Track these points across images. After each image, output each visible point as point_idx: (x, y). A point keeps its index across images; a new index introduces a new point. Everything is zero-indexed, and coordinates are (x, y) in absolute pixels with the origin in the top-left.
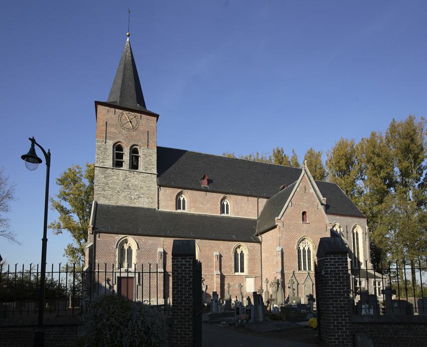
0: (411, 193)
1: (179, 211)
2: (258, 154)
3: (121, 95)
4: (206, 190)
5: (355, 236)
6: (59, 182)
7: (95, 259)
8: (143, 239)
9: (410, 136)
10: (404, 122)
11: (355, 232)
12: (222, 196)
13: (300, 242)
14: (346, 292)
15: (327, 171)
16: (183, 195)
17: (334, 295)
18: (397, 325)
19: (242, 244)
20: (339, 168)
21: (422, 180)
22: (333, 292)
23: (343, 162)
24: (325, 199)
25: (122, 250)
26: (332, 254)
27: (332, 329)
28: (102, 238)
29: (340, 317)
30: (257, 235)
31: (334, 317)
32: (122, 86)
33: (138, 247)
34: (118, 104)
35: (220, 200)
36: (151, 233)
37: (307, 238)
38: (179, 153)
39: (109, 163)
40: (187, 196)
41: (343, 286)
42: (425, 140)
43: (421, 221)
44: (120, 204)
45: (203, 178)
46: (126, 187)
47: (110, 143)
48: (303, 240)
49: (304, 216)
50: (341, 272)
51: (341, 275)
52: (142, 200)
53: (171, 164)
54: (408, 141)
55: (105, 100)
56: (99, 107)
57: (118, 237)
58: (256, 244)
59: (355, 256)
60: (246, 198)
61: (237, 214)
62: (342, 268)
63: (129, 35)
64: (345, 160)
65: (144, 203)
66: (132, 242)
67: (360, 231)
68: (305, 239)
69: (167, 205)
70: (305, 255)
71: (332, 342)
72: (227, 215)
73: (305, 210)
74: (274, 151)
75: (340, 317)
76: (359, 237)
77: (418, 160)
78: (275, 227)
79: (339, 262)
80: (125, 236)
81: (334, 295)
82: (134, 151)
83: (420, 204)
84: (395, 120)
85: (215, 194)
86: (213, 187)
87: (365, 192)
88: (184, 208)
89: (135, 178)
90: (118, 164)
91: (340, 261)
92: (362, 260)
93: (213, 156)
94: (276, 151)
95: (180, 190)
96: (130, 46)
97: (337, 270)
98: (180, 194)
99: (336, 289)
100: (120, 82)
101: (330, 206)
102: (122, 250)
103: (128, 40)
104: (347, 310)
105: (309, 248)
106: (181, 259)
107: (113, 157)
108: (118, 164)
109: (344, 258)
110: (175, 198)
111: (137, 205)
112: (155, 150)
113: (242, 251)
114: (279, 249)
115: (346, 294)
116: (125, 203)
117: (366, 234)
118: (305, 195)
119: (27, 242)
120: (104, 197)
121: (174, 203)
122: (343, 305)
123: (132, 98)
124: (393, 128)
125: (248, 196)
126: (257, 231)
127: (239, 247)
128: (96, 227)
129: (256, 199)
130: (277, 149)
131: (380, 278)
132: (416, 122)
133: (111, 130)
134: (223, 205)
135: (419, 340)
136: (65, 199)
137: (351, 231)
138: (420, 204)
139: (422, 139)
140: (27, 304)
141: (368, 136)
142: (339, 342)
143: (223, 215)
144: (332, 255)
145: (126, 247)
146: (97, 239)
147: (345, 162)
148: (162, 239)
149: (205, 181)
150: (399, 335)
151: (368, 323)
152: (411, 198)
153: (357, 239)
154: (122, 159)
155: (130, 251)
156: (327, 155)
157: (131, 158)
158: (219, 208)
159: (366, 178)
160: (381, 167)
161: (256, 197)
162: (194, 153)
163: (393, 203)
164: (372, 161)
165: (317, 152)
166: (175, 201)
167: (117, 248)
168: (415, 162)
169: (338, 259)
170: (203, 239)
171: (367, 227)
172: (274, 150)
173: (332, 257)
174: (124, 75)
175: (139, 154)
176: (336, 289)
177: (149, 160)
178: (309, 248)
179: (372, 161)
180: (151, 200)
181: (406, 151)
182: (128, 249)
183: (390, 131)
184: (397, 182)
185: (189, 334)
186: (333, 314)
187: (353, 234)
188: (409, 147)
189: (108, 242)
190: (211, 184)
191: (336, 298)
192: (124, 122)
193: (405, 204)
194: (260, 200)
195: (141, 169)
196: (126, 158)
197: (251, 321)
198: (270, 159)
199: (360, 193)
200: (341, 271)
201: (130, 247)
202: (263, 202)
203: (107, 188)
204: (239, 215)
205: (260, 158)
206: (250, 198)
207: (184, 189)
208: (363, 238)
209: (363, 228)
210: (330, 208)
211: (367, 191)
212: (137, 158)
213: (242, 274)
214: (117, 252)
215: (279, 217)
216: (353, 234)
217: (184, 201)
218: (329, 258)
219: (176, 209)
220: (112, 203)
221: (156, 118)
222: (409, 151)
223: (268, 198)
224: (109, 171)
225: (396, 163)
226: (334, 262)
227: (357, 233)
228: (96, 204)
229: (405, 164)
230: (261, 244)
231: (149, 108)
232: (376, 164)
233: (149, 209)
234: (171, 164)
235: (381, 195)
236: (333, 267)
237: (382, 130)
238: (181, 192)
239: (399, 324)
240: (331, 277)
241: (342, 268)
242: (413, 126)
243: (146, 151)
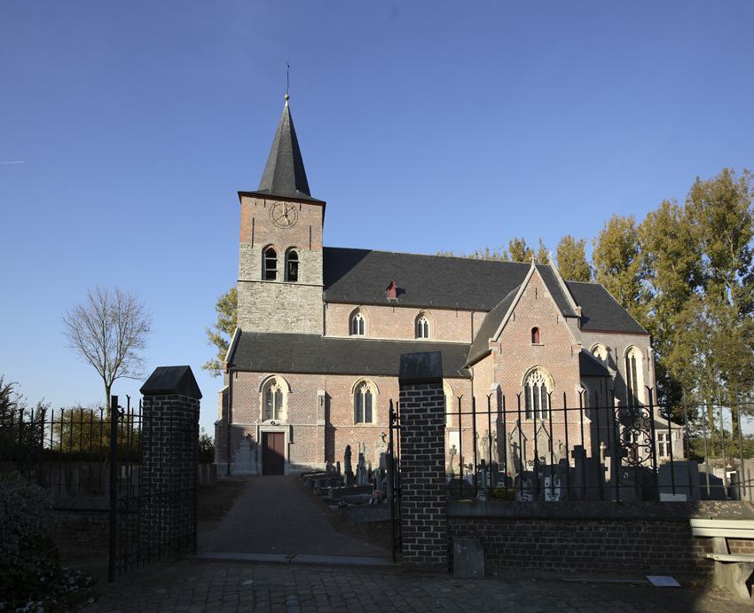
0: (729, 295)
1: (354, 336)
2: (488, 250)
3: (274, 180)
4: (393, 305)
5: (631, 364)
6: (219, 308)
7: (231, 407)
8: (297, 379)
9: (727, 200)
10: (715, 181)
11: (630, 356)
12: (417, 311)
13: (528, 375)
14: (438, 457)
15: (594, 268)
16: (360, 314)
17: (416, 463)
18: (542, 522)
19: (366, 378)
20: (611, 260)
21: (749, 271)
22: (412, 458)
23: (617, 251)
24: (580, 308)
25: (268, 395)
26: (412, 384)
27: (409, 528)
28: (242, 378)
29: (424, 505)
30: (467, 368)
31: (413, 505)
32: (276, 168)
33: (290, 389)
34: (270, 193)
35: (414, 318)
36: (307, 370)
37: (540, 369)
38: (359, 255)
39: (257, 275)
40: (366, 314)
41: (432, 445)
42: (752, 207)
43: (745, 335)
44: (272, 330)
45: (390, 287)
46: (280, 307)
47: (259, 247)
48: (533, 372)
49: (536, 335)
50: (429, 420)
51: (430, 424)
52: (302, 324)
53: (343, 269)
54: (722, 210)
55: (254, 189)
56: (244, 198)
57: (262, 376)
58: (464, 381)
59: (630, 391)
60: (453, 313)
61: (441, 337)
62: (432, 410)
63: (288, 98)
64: (620, 248)
65: (306, 327)
66: (281, 381)
67: (637, 354)
68: (536, 370)
69: (337, 329)
70: (538, 396)
71: (408, 553)
72: (426, 340)
73: (537, 325)
74: (511, 245)
75: (424, 505)
76: (638, 364)
77: (742, 239)
78: (489, 353)
79: (427, 399)
80: (269, 374)
81: (416, 463)
82: (292, 256)
83: (744, 310)
84: (700, 180)
85: (407, 310)
86: (405, 298)
87: (655, 297)
88: (362, 333)
89: (293, 293)
90: (269, 275)
91: (429, 397)
92: (642, 397)
93: (407, 255)
94: (513, 244)
95: (355, 307)
96: (290, 116)
97: (421, 414)
98: (355, 312)
99: (419, 452)
100: (274, 162)
101: (588, 319)
102: (268, 395)
103: (286, 104)
104: (439, 493)
105: (543, 384)
106: (157, 399)
107: (263, 266)
109: (436, 390)
110: (348, 318)
111: (296, 331)
113: (368, 391)
114: (494, 386)
115: (437, 461)
116: (279, 329)
117: (649, 359)
118: (533, 301)
119: (60, 384)
120: (251, 322)
121: (347, 326)
122: (431, 483)
123: (292, 183)
124: (698, 193)
125: (457, 310)
126: (468, 361)
127: (364, 383)
128: (234, 363)
129: (469, 313)
130: (516, 240)
131: (665, 428)
132: (736, 180)
133: (260, 228)
134: (420, 325)
135: (585, 550)
136: (224, 329)
137: (624, 355)
138: (744, 310)
139: (747, 206)
140: (124, 468)
141: (655, 207)
142: (420, 553)
143: (419, 339)
144: (413, 387)
145: (274, 390)
146: (234, 380)
147: (622, 252)
148: (323, 377)
149: (393, 292)
150: (544, 540)
151: (484, 518)
152: (731, 301)
153: (634, 368)
154: (275, 267)
155: (279, 395)
156: (594, 244)
157: (287, 265)
158: (414, 329)
159: (656, 274)
160: (678, 254)
161: (470, 310)
162: (380, 252)
163: (701, 309)
164: (663, 245)
165: (577, 241)
166: (348, 322)
167: (260, 391)
168: (736, 241)
169: (424, 393)
170: (383, 375)
171: (650, 349)
172: (511, 242)
173: (413, 390)
174: (279, 152)
175: (299, 260)
176: (419, 452)
177: (312, 267)
178: (543, 384)
179: (663, 245)
180: (314, 323)
181: (721, 224)
182: (276, 393)
183: (692, 196)
184: (707, 277)
185: (165, 529)
186: (411, 499)
187: (627, 360)
188: (724, 218)
189: (251, 382)
190: (403, 295)
191: (418, 469)
192: (276, 216)
193: (717, 313)
194: (476, 314)
195: (301, 279)
196: (280, 266)
197: (386, 501)
198: (506, 256)
199: (649, 297)
200: (430, 416)
201: (279, 390)
202: (480, 317)
203: (254, 310)
204: (443, 339)
205: (491, 255)
206: (459, 313)
207: (361, 304)
208: (644, 366)
209: (644, 351)
210: (589, 322)
211: (658, 294)
212: (295, 265)
213: (369, 425)
214: (261, 398)
215: (495, 338)
216: (627, 360)
217: (426, 325)
218: (406, 392)
219: (350, 334)
220: (261, 329)
221: (321, 208)
222: (724, 223)
223: (488, 312)
224: (258, 286)
225: (703, 245)
226: (417, 400)
227: (633, 359)
228: (240, 332)
229: (718, 246)
230: (472, 380)
231: (314, 195)
232: (669, 250)
233: (311, 336)
234: (343, 269)
235: (680, 298)
236: (414, 408)
237: (678, 196)
238: (357, 308)
239: (547, 519)
240: (410, 428)
241: (432, 410)
242: (730, 184)
243: (307, 254)
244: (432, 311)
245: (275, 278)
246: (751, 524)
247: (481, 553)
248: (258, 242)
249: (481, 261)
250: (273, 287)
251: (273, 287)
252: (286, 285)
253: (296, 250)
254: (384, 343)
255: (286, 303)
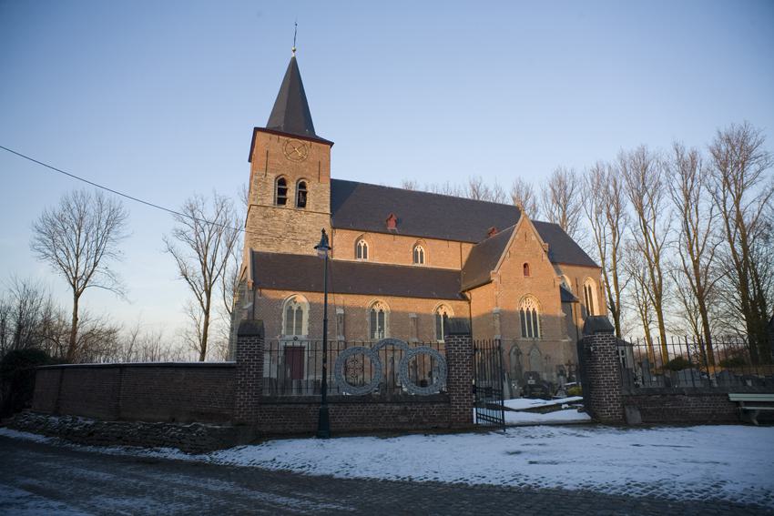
4: (394, 233)
34: (282, 130)
35: (412, 246)
44: (282, 251)
47: (272, 176)
73: (527, 262)
85: (406, 239)
86: (404, 229)
90: (282, 201)
108: (282, 201)
110: (353, 244)
112: (329, 185)
125: (448, 240)
129: (458, 244)
177: (319, 197)
194: (464, 245)
196: (292, 194)
212: (305, 194)
215: (495, 271)
230: (470, 303)
231: (319, 132)
244: (427, 240)
245: (285, 204)
246: (773, 395)
247: (638, 413)
248: (271, 172)
249: (453, 197)
250: (284, 212)
251: (284, 212)
252: (296, 211)
253: (306, 182)
254: (386, 267)
255: (296, 227)
